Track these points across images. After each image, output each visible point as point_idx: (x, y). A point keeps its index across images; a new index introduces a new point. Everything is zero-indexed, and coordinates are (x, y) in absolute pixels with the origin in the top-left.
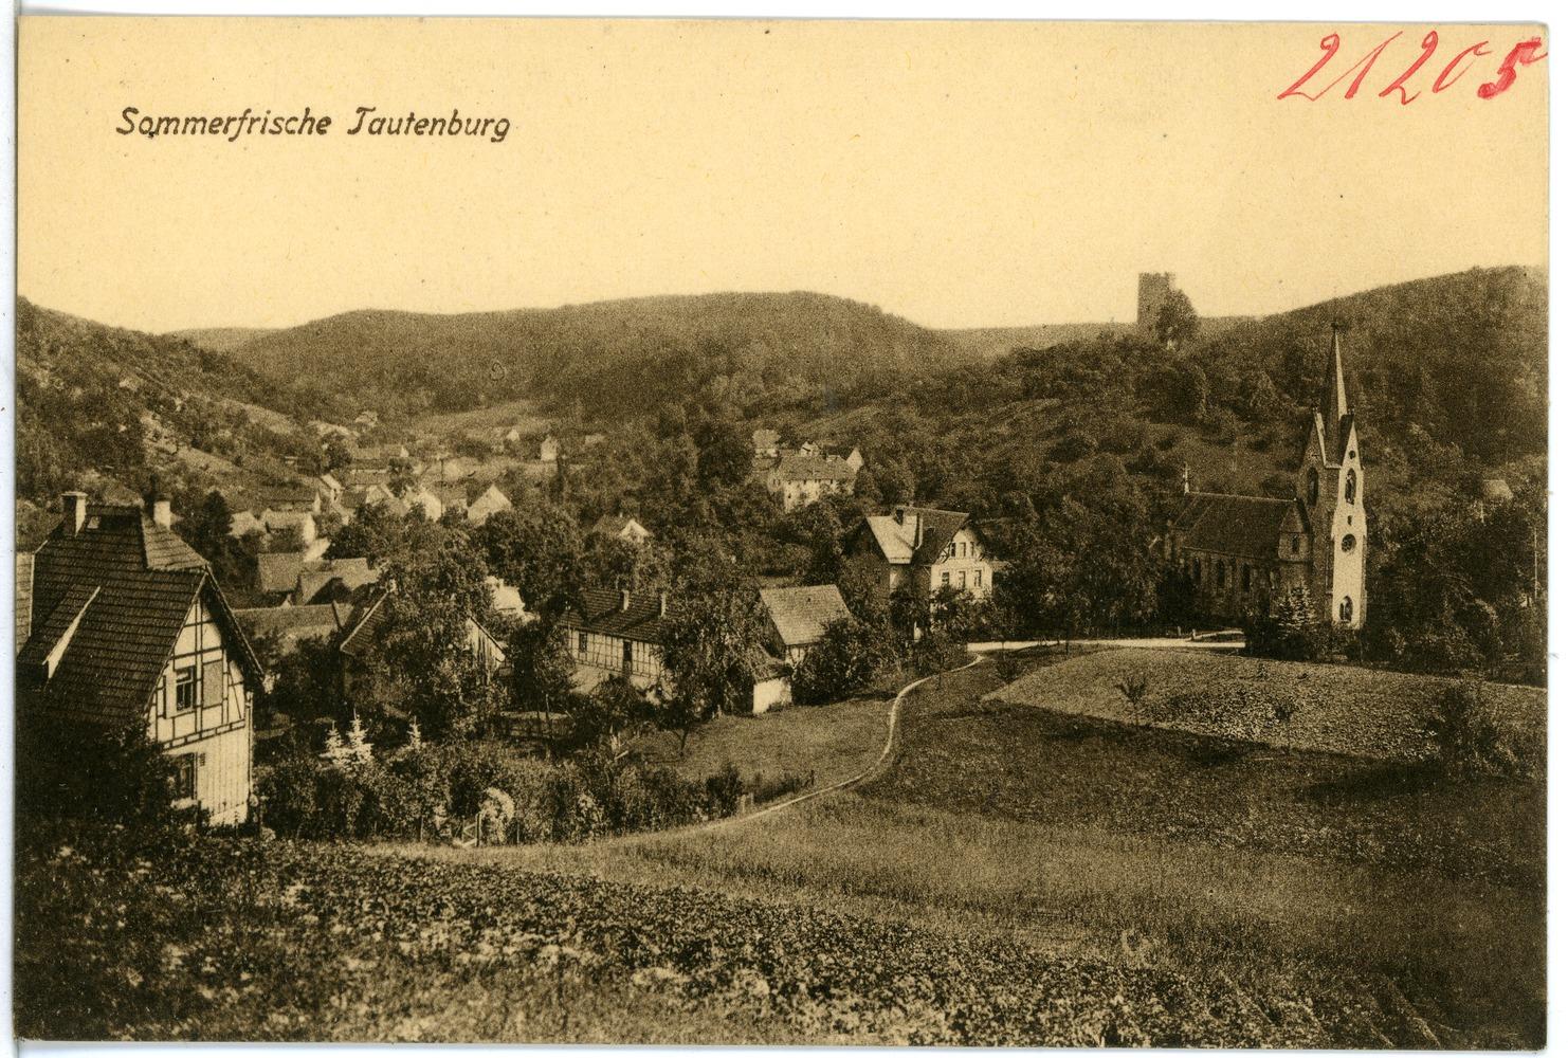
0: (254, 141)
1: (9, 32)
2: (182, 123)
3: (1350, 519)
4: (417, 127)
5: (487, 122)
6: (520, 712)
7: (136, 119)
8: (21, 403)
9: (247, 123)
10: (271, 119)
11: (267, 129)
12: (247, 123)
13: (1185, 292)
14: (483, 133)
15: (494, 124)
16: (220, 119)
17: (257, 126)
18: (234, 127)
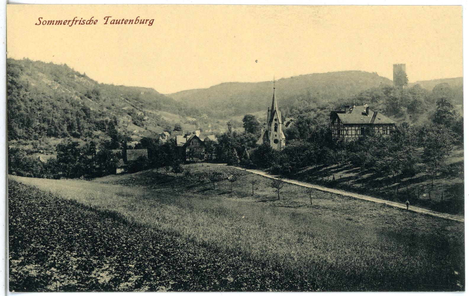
0: (76, 26)
1: (2, 24)
2: (47, 22)
3: (379, 119)
4: (125, 22)
5: (147, 20)
6: (236, 166)
7: (42, 20)
8: (318, 289)
9: (75, 22)
10: (82, 20)
11: (81, 23)
12: (75, 22)
13: (374, 71)
14: (146, 23)
15: (149, 21)
16: (128, 20)
17: (78, 22)
18: (71, 23)
